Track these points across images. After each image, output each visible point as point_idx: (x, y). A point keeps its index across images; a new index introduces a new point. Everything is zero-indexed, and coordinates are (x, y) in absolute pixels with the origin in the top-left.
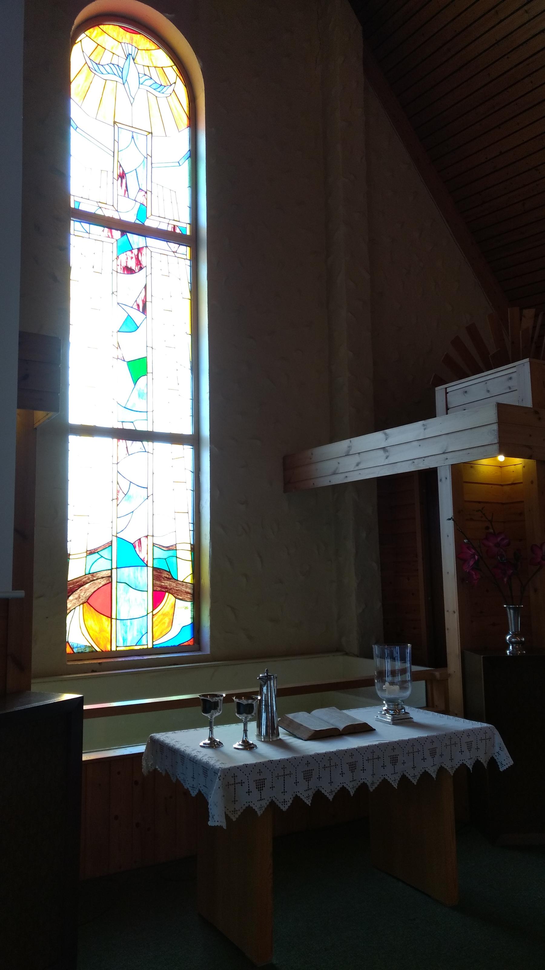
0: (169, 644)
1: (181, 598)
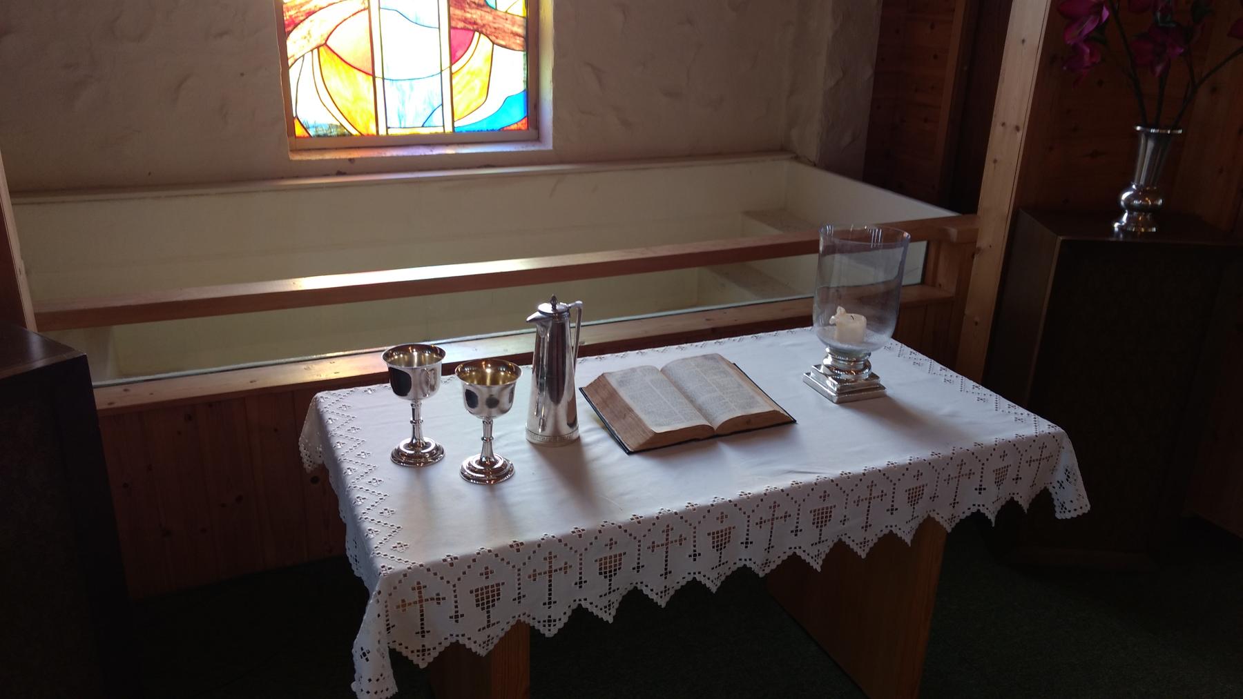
0: (484, 127)
1: (503, 43)
